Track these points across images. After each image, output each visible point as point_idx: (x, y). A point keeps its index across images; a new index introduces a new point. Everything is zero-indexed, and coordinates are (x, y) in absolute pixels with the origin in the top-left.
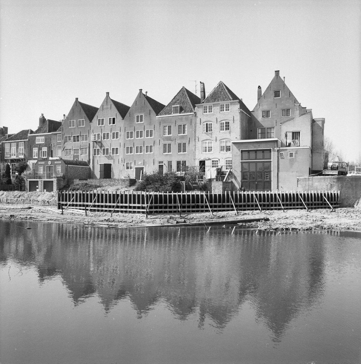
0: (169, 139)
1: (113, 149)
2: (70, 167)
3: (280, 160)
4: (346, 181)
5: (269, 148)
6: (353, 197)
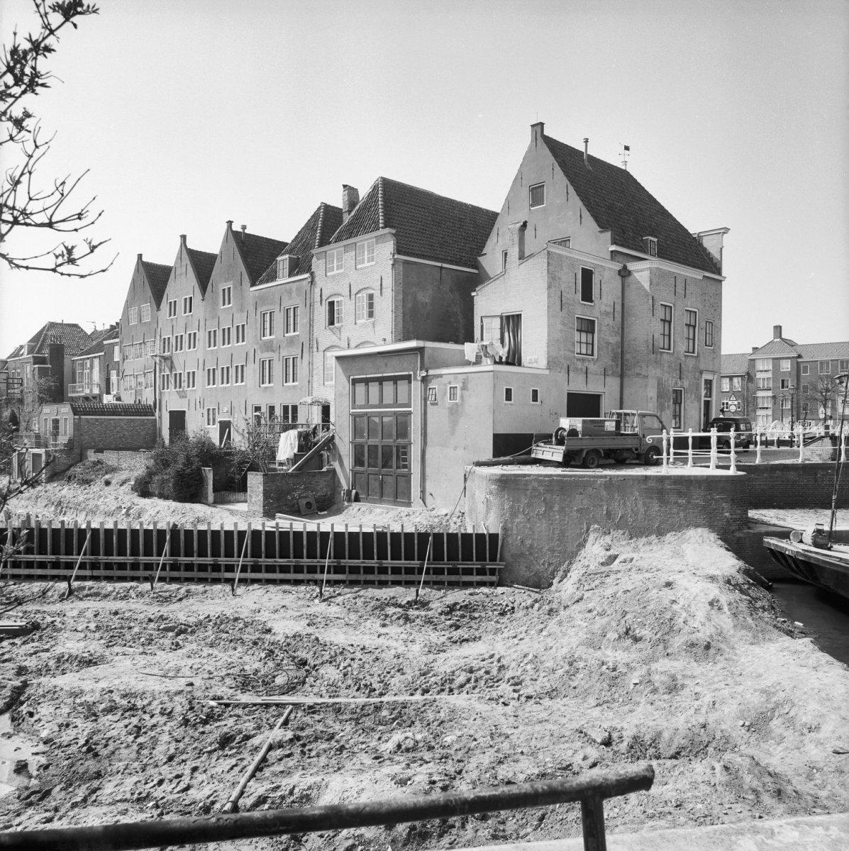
0: (269, 347)
1: (189, 373)
2: (88, 422)
3: (430, 409)
4: (528, 493)
5: (407, 373)
6: (552, 550)
